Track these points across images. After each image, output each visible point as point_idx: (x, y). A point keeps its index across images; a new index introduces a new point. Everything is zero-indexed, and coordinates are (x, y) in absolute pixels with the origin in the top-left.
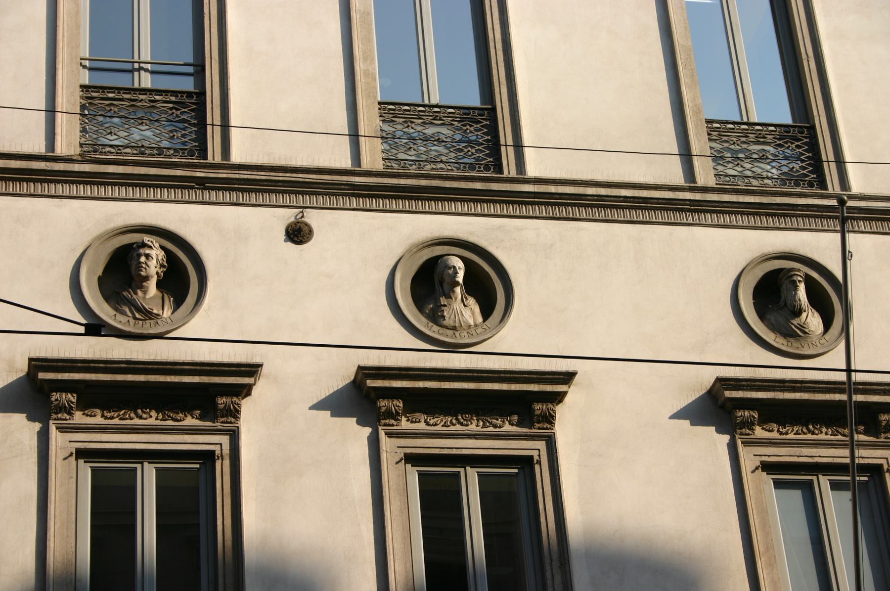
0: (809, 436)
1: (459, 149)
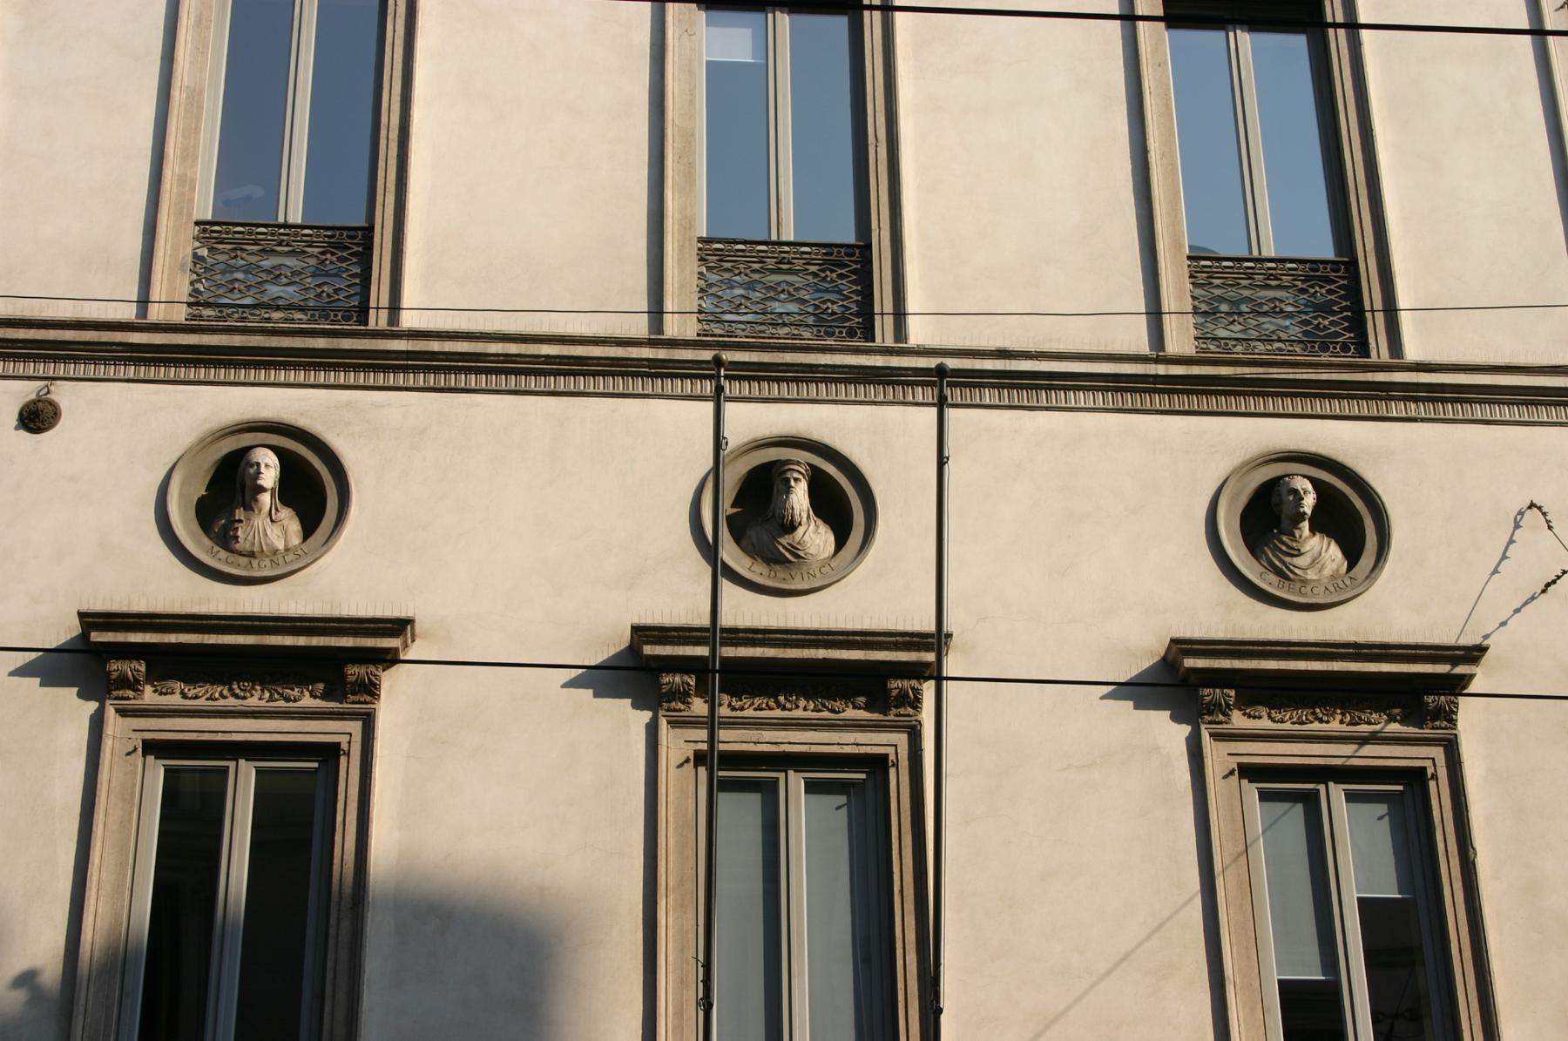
0: (778, 713)
1: (804, 297)
